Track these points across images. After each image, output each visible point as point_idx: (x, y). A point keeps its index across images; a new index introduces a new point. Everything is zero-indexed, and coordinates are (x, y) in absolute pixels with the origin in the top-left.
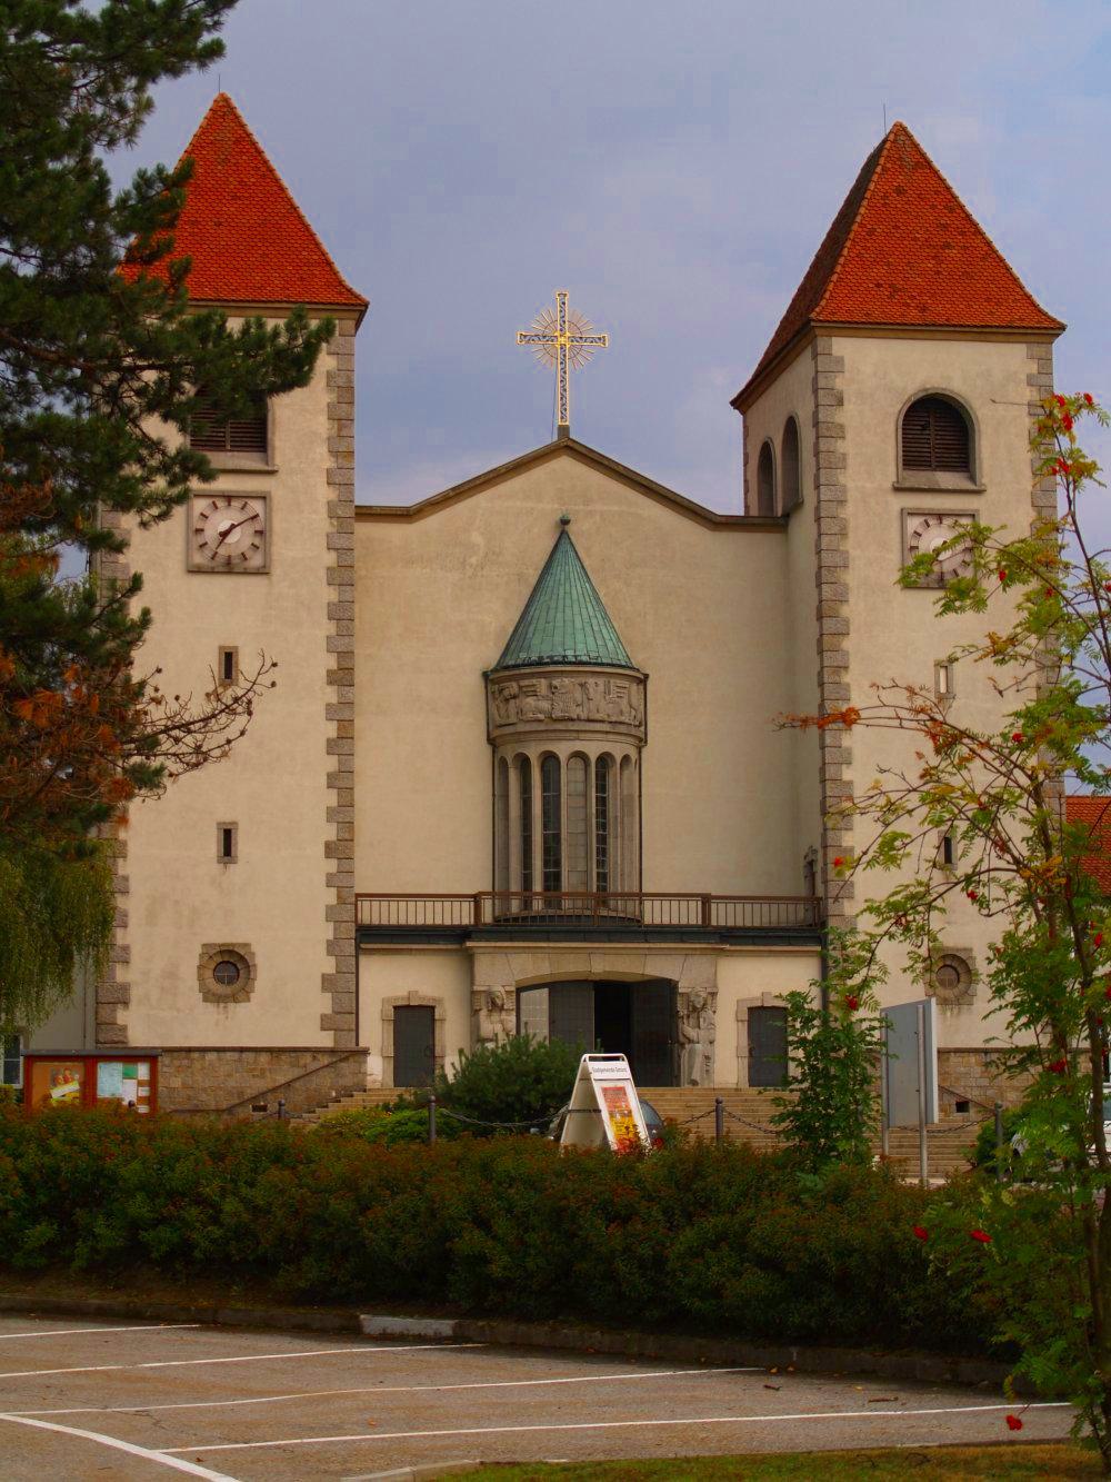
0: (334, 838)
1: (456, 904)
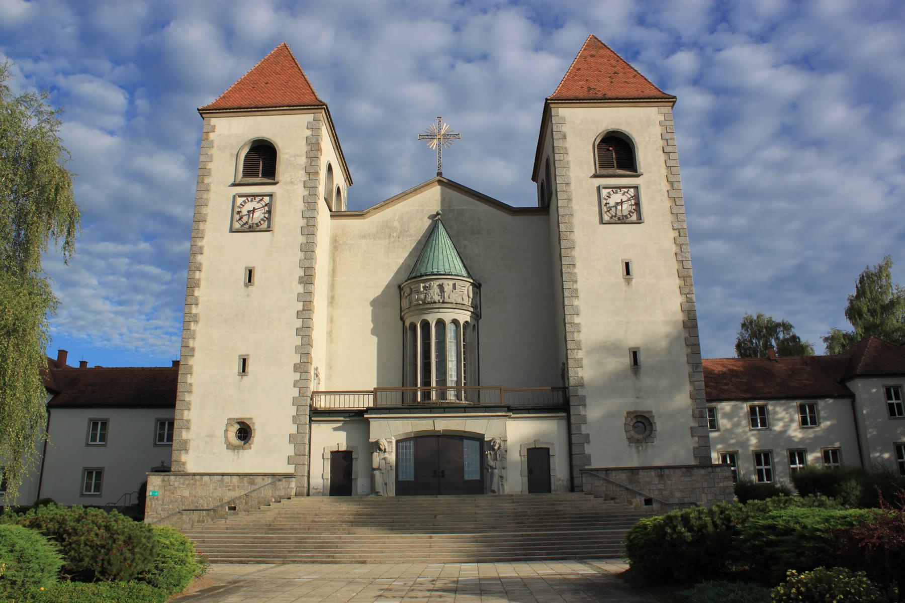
0: (298, 361)
1: (361, 396)
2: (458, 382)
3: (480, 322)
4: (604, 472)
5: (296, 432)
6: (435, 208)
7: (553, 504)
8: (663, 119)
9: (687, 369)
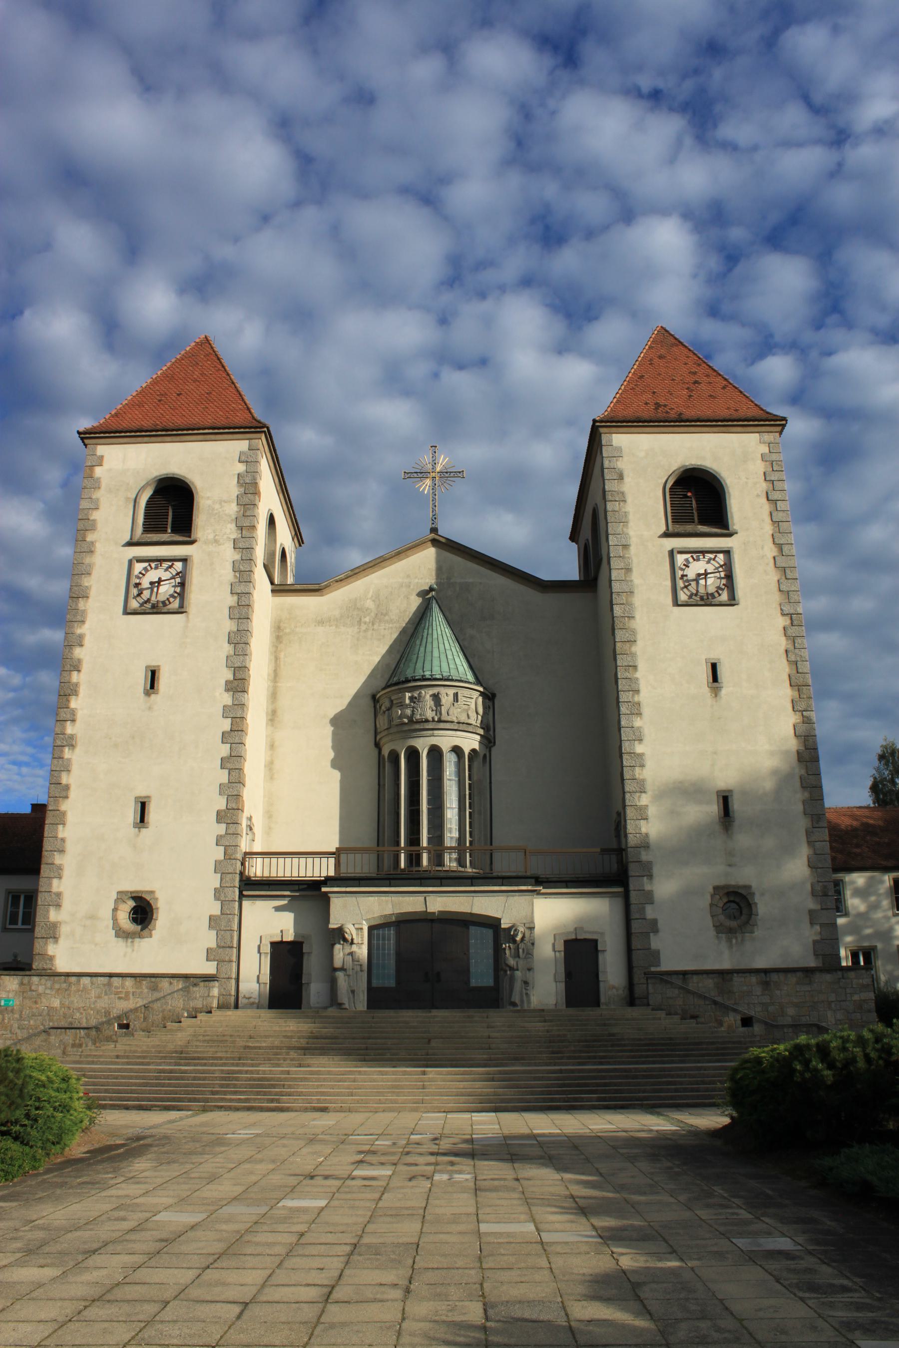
0: (224, 807)
1: (317, 860)
2: (461, 839)
3: (493, 749)
4: (681, 976)
5: (219, 913)
6: (427, 581)
7: (605, 1025)
8: (767, 451)
9: (802, 823)
